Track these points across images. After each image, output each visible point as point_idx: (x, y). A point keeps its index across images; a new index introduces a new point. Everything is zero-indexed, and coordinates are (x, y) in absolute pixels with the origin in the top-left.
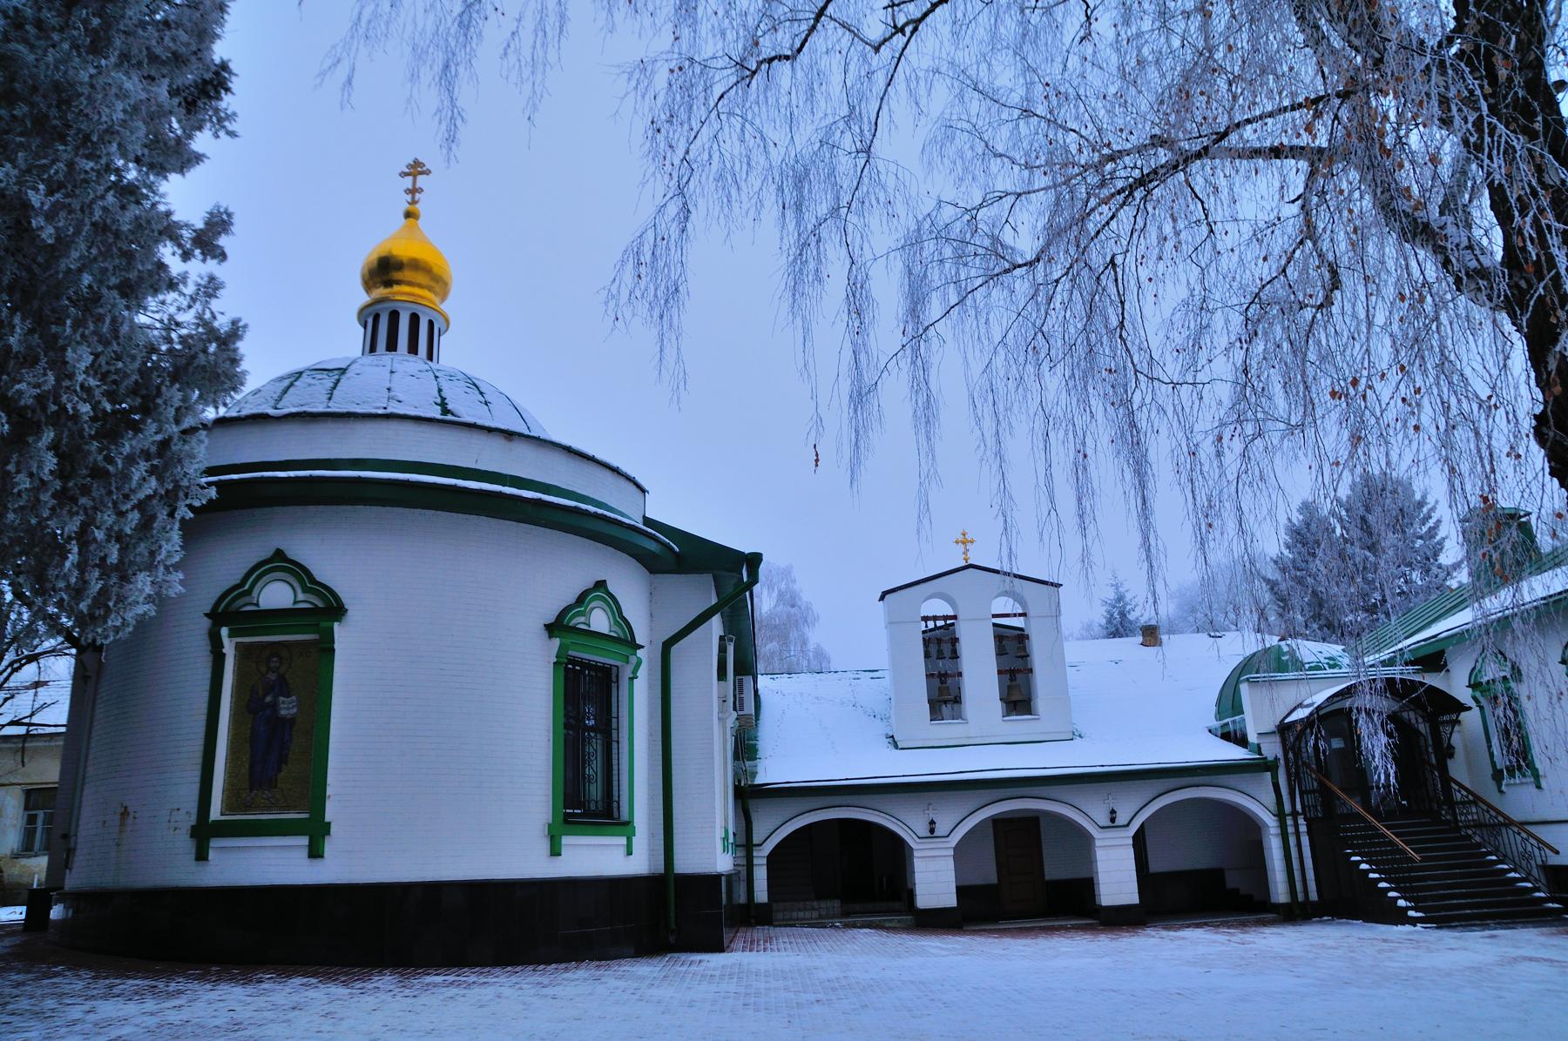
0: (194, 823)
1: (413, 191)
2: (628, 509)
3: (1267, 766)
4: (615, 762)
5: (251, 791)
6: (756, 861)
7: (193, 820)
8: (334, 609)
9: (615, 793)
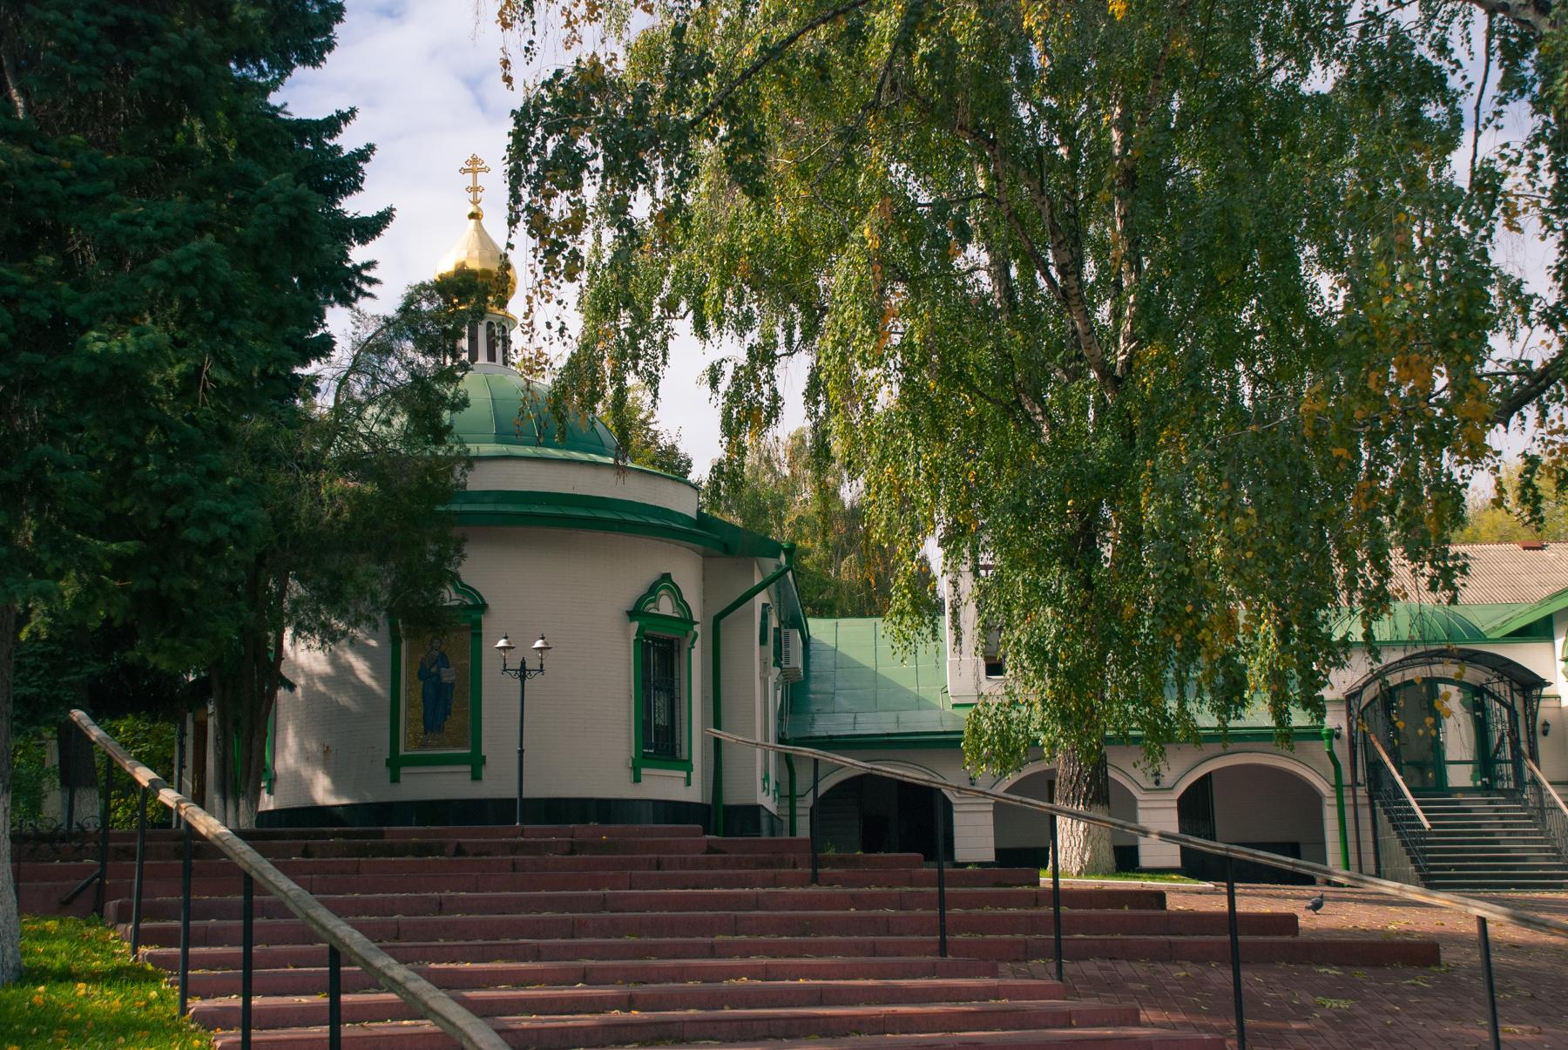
1: (475, 189)
6: (798, 812)
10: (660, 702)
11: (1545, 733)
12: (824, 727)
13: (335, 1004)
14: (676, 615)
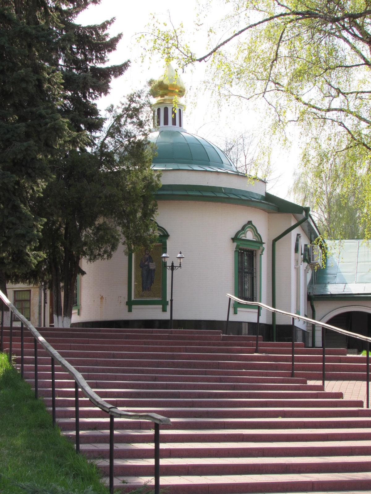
0: (127, 301)
2: (259, 190)
4: (255, 284)
5: (143, 291)
7: (126, 300)
9: (255, 295)
10: (247, 279)
12: (333, 289)
13: (36, 367)
14: (254, 240)
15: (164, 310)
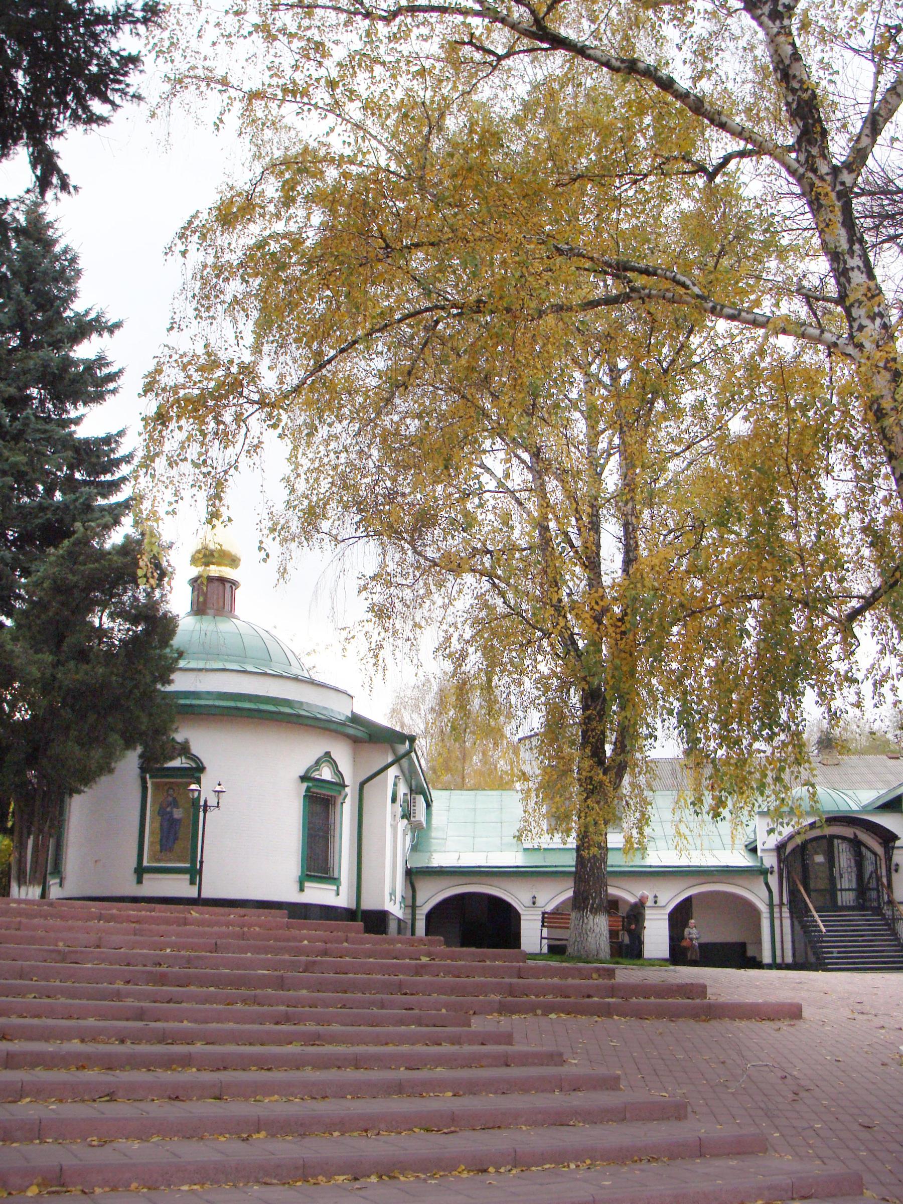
2: (340, 709)
3: (764, 872)
8: (201, 769)
11: (896, 871)
12: (440, 859)
15: (192, 882)
